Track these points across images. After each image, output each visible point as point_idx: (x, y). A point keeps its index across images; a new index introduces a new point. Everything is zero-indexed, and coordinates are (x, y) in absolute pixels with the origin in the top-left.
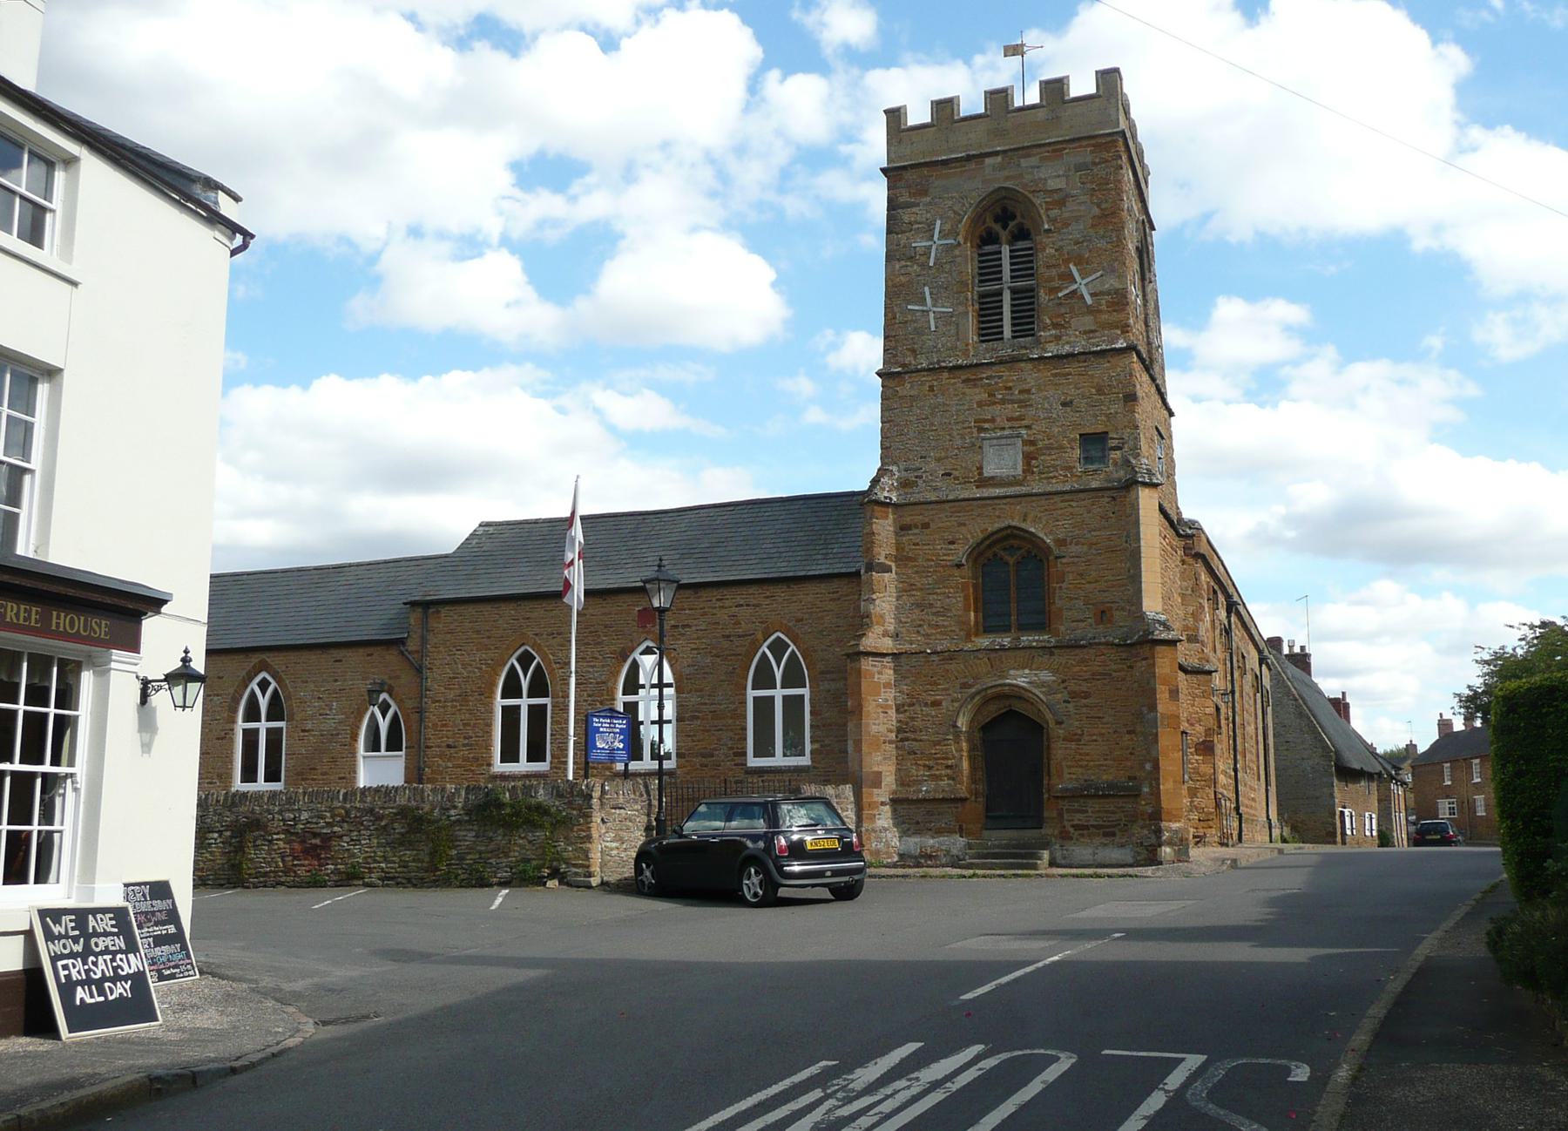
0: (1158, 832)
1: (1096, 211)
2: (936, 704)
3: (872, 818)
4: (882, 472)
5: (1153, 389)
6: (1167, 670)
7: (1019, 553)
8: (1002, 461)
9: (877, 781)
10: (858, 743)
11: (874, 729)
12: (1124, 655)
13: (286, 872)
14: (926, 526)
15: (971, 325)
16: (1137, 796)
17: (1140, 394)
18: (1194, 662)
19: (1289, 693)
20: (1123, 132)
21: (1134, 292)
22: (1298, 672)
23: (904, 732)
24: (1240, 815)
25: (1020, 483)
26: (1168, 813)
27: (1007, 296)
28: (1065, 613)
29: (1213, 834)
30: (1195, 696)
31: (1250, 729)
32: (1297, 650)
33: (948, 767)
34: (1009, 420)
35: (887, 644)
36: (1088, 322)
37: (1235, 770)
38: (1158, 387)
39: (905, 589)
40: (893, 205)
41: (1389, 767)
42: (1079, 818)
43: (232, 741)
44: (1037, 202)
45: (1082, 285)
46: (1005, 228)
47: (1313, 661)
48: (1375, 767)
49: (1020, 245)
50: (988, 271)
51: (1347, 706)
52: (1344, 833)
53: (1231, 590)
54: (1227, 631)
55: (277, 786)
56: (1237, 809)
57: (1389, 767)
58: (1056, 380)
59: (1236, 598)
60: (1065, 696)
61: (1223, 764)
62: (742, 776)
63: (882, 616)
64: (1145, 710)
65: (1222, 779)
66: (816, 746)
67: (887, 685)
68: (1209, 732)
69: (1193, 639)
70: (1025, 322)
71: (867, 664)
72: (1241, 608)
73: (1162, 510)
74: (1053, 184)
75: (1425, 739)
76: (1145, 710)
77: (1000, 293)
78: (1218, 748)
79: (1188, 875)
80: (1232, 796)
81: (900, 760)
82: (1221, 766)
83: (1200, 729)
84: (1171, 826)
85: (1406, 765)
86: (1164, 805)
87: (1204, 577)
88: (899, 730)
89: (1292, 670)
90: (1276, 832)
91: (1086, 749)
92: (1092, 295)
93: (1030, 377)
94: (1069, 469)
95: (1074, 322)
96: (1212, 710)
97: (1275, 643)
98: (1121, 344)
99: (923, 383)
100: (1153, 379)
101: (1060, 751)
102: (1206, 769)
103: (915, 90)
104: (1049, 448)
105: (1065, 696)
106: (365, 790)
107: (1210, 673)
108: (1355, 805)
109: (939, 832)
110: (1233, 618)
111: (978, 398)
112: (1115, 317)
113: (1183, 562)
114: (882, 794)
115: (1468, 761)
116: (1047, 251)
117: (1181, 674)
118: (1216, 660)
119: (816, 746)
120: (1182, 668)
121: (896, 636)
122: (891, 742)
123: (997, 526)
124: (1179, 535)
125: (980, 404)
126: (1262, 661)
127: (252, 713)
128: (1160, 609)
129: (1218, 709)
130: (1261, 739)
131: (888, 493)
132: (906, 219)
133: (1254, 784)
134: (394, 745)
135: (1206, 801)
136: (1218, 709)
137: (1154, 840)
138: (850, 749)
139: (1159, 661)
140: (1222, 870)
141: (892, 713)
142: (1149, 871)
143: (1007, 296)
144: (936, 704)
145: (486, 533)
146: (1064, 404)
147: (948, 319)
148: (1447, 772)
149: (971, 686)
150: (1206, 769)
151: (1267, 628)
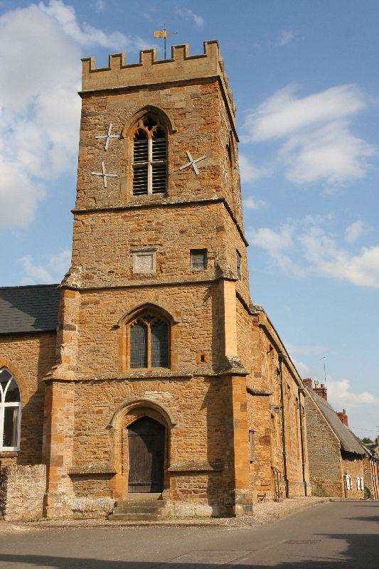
0: (233, 495)
1: (203, 121)
2: (100, 412)
3: (55, 487)
4: (73, 269)
5: (235, 228)
9: (60, 462)
10: (49, 437)
11: (59, 428)
12: (214, 383)
15: (130, 184)
16: (221, 471)
17: (227, 228)
22: (321, 399)
23: (80, 431)
25: (153, 277)
26: (240, 482)
27: (150, 169)
28: (179, 356)
29: (270, 495)
30: (258, 409)
32: (319, 387)
33: (106, 452)
35: (71, 375)
36: (196, 184)
38: (238, 228)
39: (85, 341)
41: (369, 451)
42: (185, 486)
46: (150, 129)
47: (328, 392)
49: (159, 140)
50: (141, 153)
51: (346, 417)
54: (279, 372)
56: (285, 476)
57: (369, 451)
59: (285, 354)
60: (176, 408)
61: (276, 449)
63: (68, 357)
64: (226, 417)
66: (24, 439)
67: (70, 401)
68: (267, 430)
69: (258, 375)
71: (56, 387)
73: (238, 296)
74: (178, 105)
76: (226, 417)
77: (146, 167)
78: (273, 440)
80: (282, 469)
81: (76, 449)
82: (275, 452)
84: (240, 492)
86: (237, 477)
88: (77, 429)
89: (316, 397)
90: (309, 489)
91: (189, 441)
92: (200, 169)
93: (163, 215)
96: (268, 418)
98: (215, 197)
99: (99, 218)
100: (235, 222)
103: (341, 459)
104: (173, 257)
105: (176, 408)
107: (268, 395)
109: (98, 495)
110: (301, 394)
111: (131, 227)
112: (212, 182)
113: (253, 330)
114: (63, 471)
118: (273, 387)
119: (24, 439)
120: (249, 391)
122: (70, 437)
126: (300, 391)
128: (236, 355)
129: (272, 417)
131: (75, 281)
132: (92, 121)
133: (295, 461)
136: (272, 417)
139: (234, 386)
141: (72, 418)
142: (226, 521)
143: (150, 169)
144: (100, 412)
146: (182, 232)
149: (122, 401)
150: (264, 454)
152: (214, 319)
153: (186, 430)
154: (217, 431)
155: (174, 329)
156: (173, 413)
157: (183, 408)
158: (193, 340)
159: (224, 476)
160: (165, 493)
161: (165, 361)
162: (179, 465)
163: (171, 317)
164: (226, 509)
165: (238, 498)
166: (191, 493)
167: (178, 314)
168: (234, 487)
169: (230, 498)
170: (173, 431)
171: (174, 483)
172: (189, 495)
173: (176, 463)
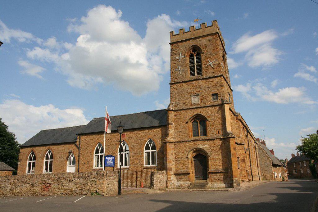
0: (232, 180)
1: (213, 48)
2: (183, 152)
3: (170, 178)
4: (171, 104)
6: (233, 144)
7: (200, 119)
8: (195, 101)
10: (166, 161)
13: (42, 192)
14: (180, 115)
18: (239, 142)
19: (261, 149)
20: (218, 32)
21: (222, 65)
22: (263, 145)
23: (177, 159)
24: (252, 175)
25: (199, 105)
27: (196, 67)
28: (210, 132)
29: (246, 180)
31: (254, 157)
33: (186, 166)
34: (197, 92)
35: (172, 140)
36: (212, 71)
37: (251, 165)
39: (176, 128)
40: (172, 50)
42: (215, 177)
43: (43, 164)
44: (201, 48)
45: (211, 63)
46: (194, 53)
48: (279, 164)
50: (192, 61)
51: (273, 152)
52: (275, 178)
53: (247, 128)
54: (247, 136)
55: (154, 165)
56: (251, 174)
57: (283, 164)
58: (207, 83)
61: (247, 163)
62: (143, 169)
65: (248, 167)
66: (158, 162)
68: (244, 157)
69: (239, 137)
70: (200, 72)
72: (250, 131)
73: (230, 109)
74: (204, 44)
75: (289, 158)
77: (194, 66)
79: (239, 190)
80: (250, 171)
81: (176, 165)
82: (247, 165)
83: (242, 157)
84: (235, 179)
85: (286, 163)
86: (234, 174)
87: (241, 125)
89: (261, 145)
90: (261, 178)
93: (201, 82)
94: (210, 101)
95: (210, 71)
97: (258, 139)
98: (219, 75)
100: (227, 83)
101: (210, 162)
102: (243, 165)
106: (68, 173)
107: (243, 144)
108: (277, 172)
109: (184, 181)
114: (172, 173)
115: (298, 162)
116: (203, 57)
117: (236, 145)
119: (158, 162)
120: (236, 143)
121: (174, 138)
123: (195, 114)
124: (235, 116)
125: (191, 89)
126: (255, 143)
127: (47, 158)
129: (245, 152)
130: (256, 159)
131: (172, 108)
134: (74, 163)
135: (244, 172)
138: (165, 163)
140: (251, 182)
141: (174, 154)
142: (231, 189)
143: (196, 67)
144: (183, 152)
145: (96, 121)
146: (208, 88)
147: (184, 73)
148: (300, 164)
150: (243, 165)
151: (256, 136)
152: (222, 118)
154: (225, 158)
155: (208, 122)
156: (209, 152)
157: (212, 150)
158: (215, 126)
160: (208, 180)
161: (205, 134)
162: (213, 170)
163: (206, 118)
164: (230, 185)
165: (234, 181)
167: (209, 117)
168: (233, 177)
170: (209, 158)
171: (211, 177)
173: (211, 169)
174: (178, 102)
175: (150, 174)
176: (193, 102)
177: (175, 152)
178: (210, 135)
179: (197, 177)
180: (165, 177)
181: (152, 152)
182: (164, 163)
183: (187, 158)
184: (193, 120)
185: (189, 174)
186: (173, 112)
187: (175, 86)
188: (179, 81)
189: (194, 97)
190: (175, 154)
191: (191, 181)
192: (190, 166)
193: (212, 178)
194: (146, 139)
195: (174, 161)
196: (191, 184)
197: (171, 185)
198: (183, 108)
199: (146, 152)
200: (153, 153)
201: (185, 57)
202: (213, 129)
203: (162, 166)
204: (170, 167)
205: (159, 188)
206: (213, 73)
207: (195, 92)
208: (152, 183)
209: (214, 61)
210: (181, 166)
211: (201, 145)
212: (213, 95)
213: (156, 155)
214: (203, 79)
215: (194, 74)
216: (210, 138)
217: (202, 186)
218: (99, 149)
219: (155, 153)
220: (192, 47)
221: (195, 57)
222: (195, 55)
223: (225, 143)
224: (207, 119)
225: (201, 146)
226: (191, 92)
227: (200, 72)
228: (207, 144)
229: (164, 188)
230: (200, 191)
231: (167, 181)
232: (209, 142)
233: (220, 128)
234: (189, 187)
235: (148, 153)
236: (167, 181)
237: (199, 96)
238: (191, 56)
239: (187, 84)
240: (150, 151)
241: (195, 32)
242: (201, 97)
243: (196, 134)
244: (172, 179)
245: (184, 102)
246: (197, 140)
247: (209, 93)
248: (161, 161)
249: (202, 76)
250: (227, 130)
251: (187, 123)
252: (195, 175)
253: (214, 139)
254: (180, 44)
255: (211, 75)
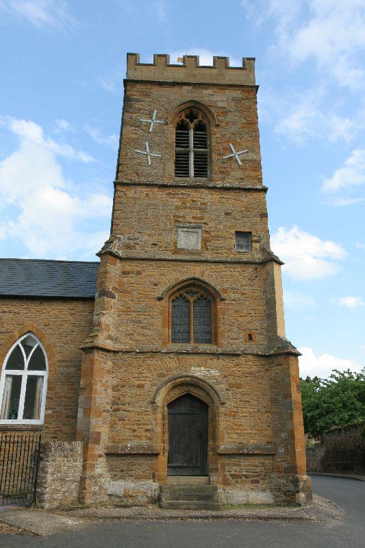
1: (243, 121)
3: (93, 467)
8: (189, 241)
14: (139, 273)
23: (117, 405)
35: (109, 344)
36: (239, 174)
42: (234, 470)
45: (238, 155)
50: (181, 140)
66: (50, 412)
70: (201, 170)
74: (220, 104)
76: (280, 398)
77: (187, 154)
81: (112, 426)
101: (223, 423)
109: (138, 478)
114: (100, 449)
116: (216, 136)
123: (185, 277)
137: (292, 488)
141: (110, 391)
144: (141, 386)
147: (157, 159)
153: (235, 410)
154: (267, 412)
155: (220, 306)
158: (240, 319)
159: (279, 460)
160: (214, 478)
166: (241, 478)
167: (225, 291)
169: (291, 484)
171: (223, 467)
172: (239, 480)
173: (225, 445)
174: (137, 235)
175: (34, 446)
176: (181, 244)
177: (115, 382)
178: (226, 344)
179: (173, 467)
180: (79, 464)
181: (29, 376)
182: (75, 417)
183: (153, 402)
184: (177, 295)
185: (157, 455)
186: (119, 264)
187: (131, 192)
188: (143, 180)
189: (185, 229)
190: (115, 388)
191: (159, 480)
192: (153, 430)
193: (227, 473)
194: (16, 334)
195: (108, 411)
196: (161, 488)
197: (95, 493)
198: (150, 255)
199: (7, 376)
200: (32, 381)
201: (167, 124)
202: (234, 323)
203: (70, 421)
204: (98, 430)
205: (56, 504)
206: (241, 179)
207: (189, 218)
208: (37, 482)
209: (245, 151)
210: (130, 429)
211: (198, 369)
212: (238, 233)
213: (43, 389)
214: (214, 188)
215: (187, 174)
216: (229, 349)
217: (200, 498)
218: (25, 355)
219: (40, 380)
220: (187, 105)
221: (191, 133)
222: (192, 125)
223: (267, 370)
224: (220, 295)
225: (199, 372)
226: (179, 217)
227: (201, 170)
228: (216, 368)
229: (72, 503)
230: (213, 517)
231: (83, 480)
232: (222, 362)
233: (257, 325)
234: (156, 501)
235: (17, 380)
236: (83, 480)
237: (199, 231)
238: (182, 127)
239: (167, 194)
240: (25, 374)
241: (197, 71)
242: (206, 235)
243: (180, 335)
244: (98, 471)
245: (155, 239)
246: (188, 353)
247: (227, 229)
248: (58, 409)
249: (211, 180)
250: (278, 334)
251: (160, 299)
252: (169, 462)
253: (239, 355)
254: (156, 91)
255: (236, 184)
